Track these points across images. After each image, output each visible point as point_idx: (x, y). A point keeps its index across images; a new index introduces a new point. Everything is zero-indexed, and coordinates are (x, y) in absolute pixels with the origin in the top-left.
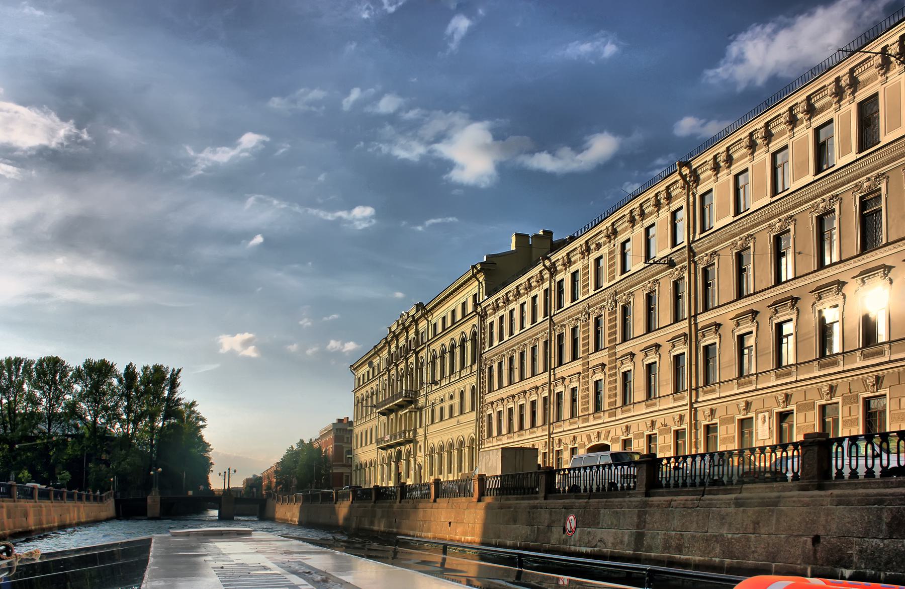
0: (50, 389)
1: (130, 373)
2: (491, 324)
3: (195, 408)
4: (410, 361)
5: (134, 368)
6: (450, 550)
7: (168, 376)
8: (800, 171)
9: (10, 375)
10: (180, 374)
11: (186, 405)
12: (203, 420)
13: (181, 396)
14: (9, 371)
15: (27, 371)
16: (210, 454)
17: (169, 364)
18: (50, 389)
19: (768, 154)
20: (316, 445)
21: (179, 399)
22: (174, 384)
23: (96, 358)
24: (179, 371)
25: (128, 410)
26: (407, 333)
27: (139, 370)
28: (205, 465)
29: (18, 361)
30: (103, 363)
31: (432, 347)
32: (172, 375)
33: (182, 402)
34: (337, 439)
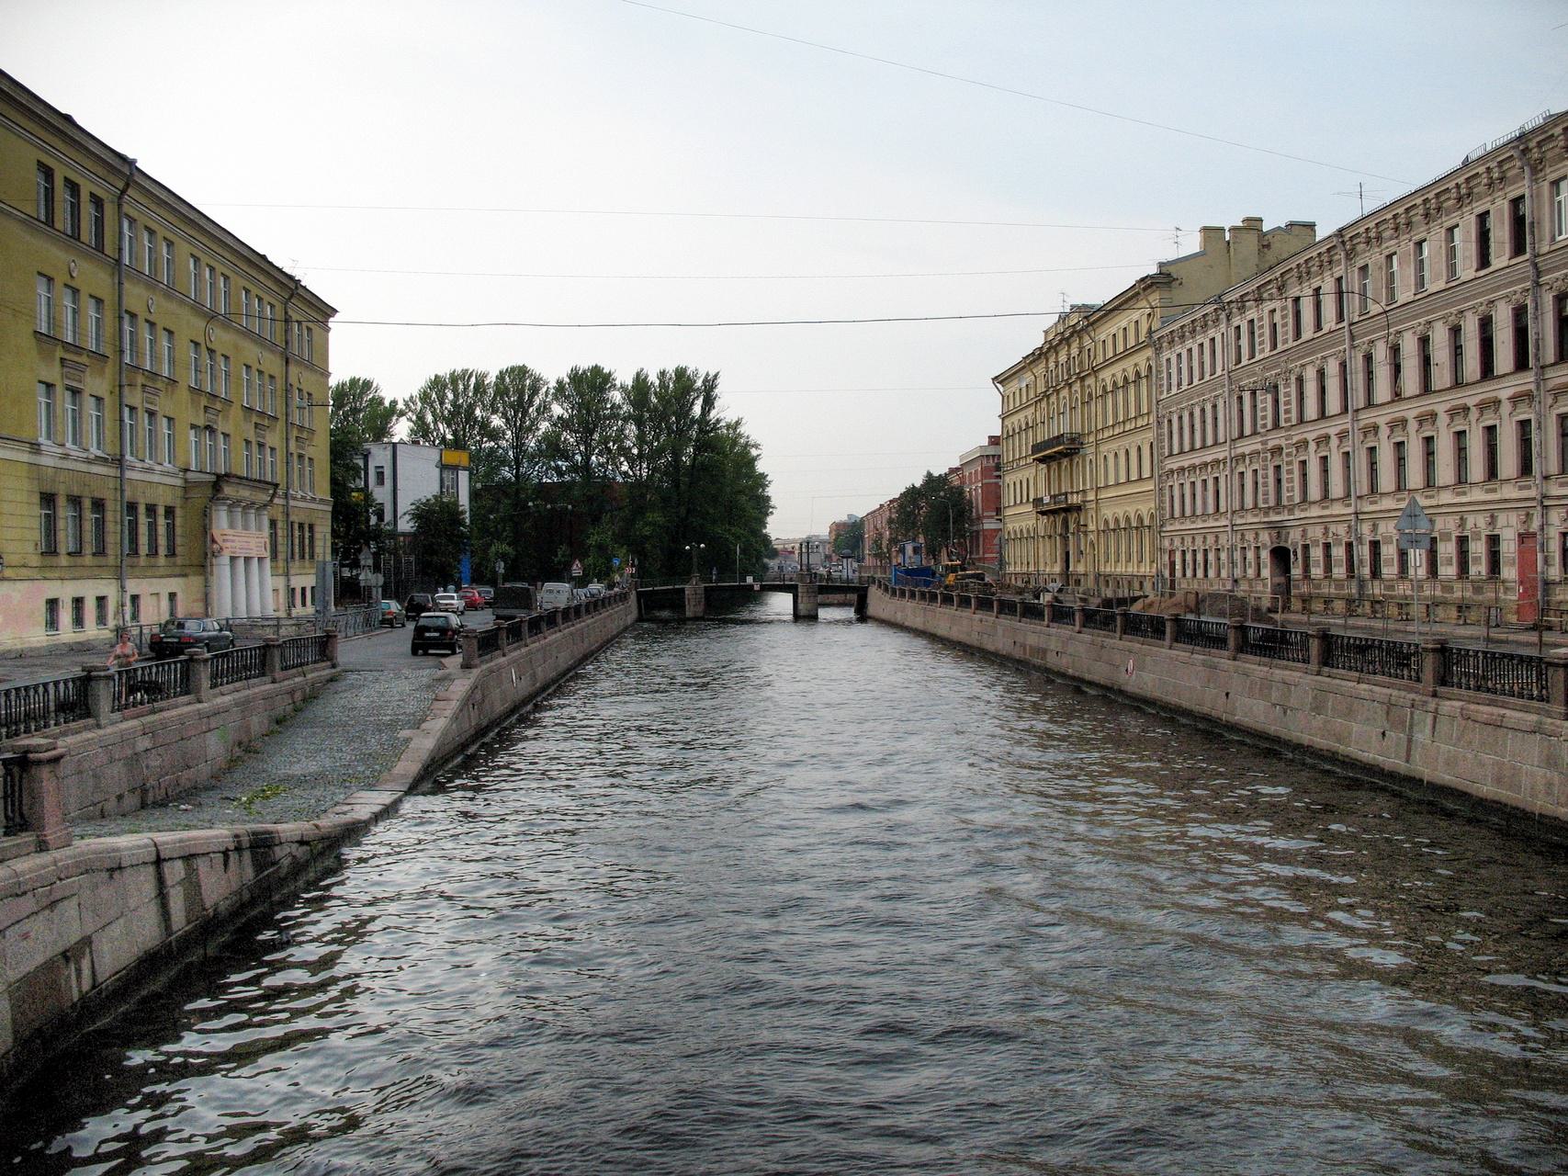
0: (516, 415)
1: (640, 382)
2: (1168, 360)
3: (741, 429)
4: (1074, 389)
5: (646, 377)
6: (131, 801)
7: (699, 383)
8: (1436, 278)
9: (456, 396)
10: (718, 381)
11: (728, 427)
12: (756, 446)
13: (721, 416)
14: (455, 391)
15: (480, 387)
16: (724, 411)
17: (700, 366)
18: (516, 415)
19: (1411, 244)
20: (955, 480)
21: (718, 421)
22: (709, 403)
23: (585, 364)
24: (716, 376)
25: (641, 439)
26: (1069, 346)
27: (653, 378)
28: (762, 506)
29: (465, 375)
30: (596, 370)
31: (1102, 375)
32: (706, 380)
33: (723, 424)
34: (986, 472)
